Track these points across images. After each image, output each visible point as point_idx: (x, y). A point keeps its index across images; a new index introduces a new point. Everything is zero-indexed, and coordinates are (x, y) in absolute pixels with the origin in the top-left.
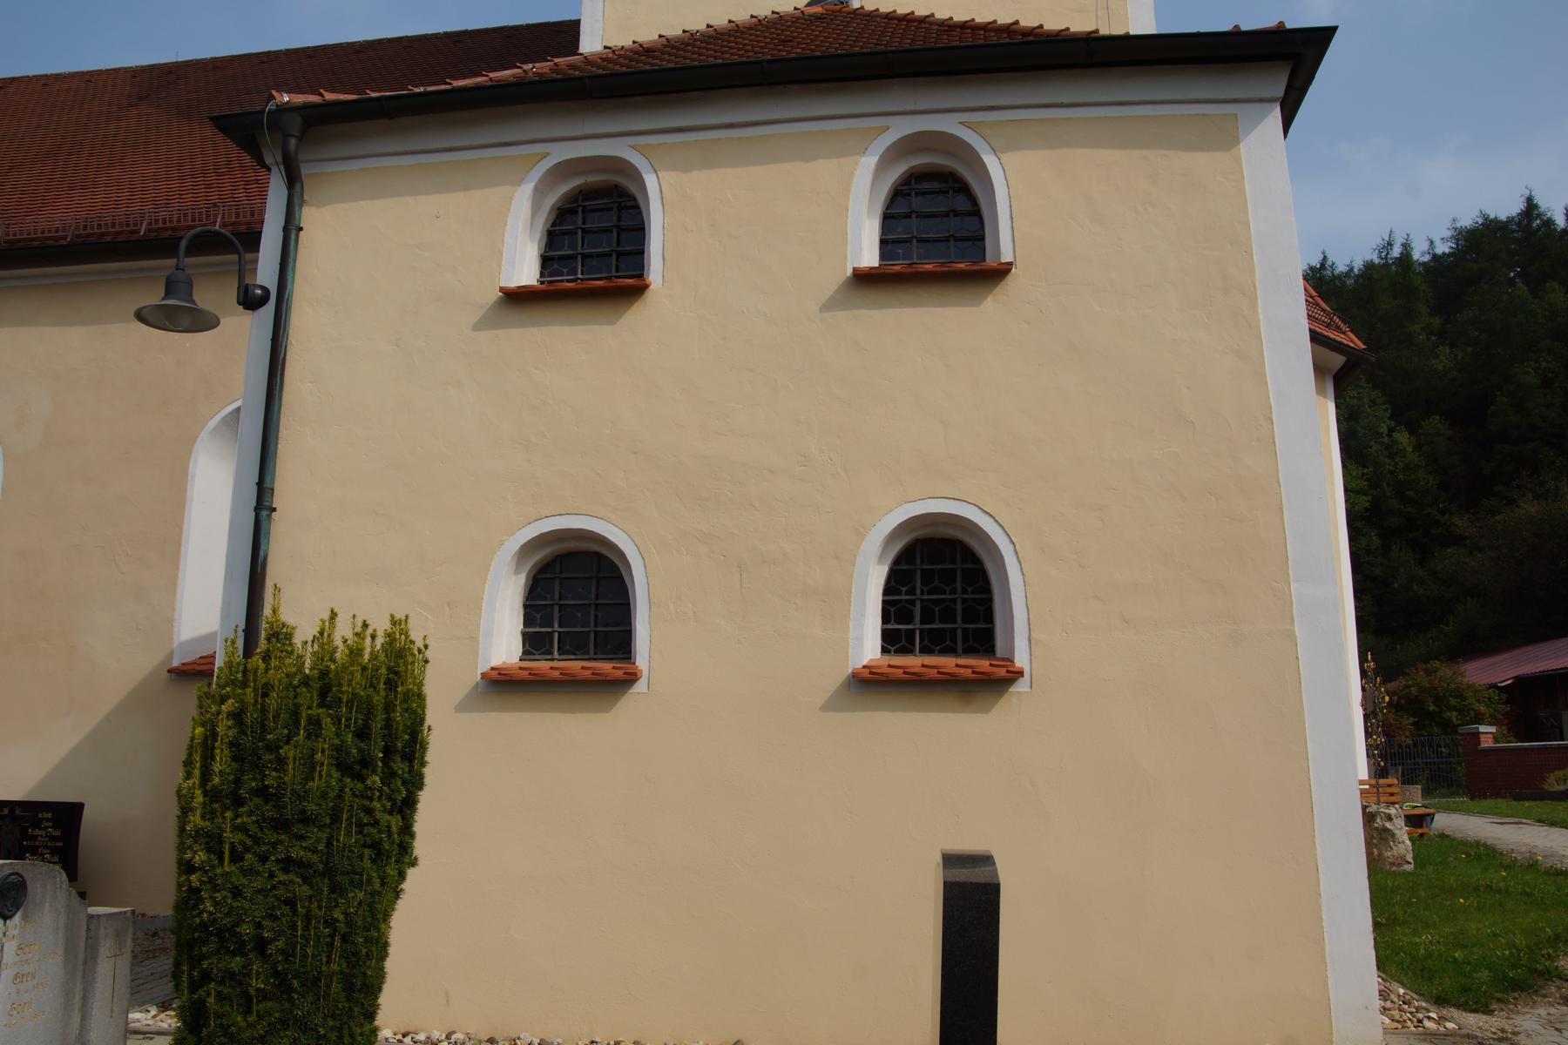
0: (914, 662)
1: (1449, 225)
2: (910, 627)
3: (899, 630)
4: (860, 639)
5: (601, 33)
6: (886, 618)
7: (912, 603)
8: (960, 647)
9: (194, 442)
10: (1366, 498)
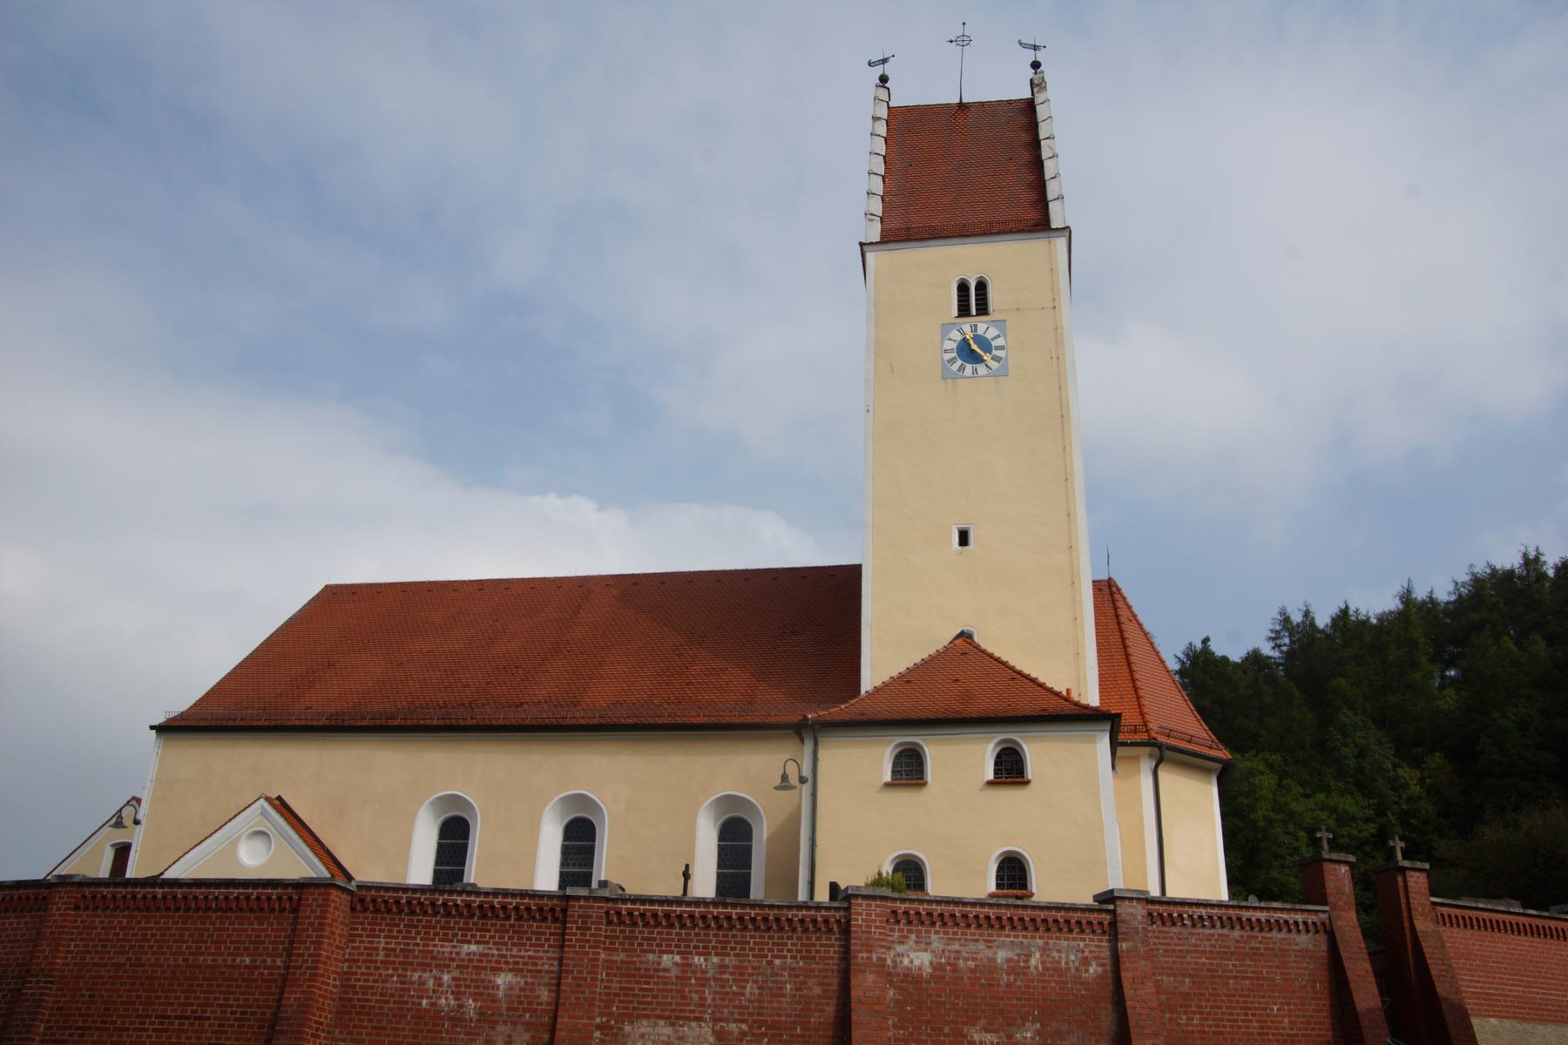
0: (1005, 891)
1: (1467, 571)
6: (997, 880)
10: (1372, 825)
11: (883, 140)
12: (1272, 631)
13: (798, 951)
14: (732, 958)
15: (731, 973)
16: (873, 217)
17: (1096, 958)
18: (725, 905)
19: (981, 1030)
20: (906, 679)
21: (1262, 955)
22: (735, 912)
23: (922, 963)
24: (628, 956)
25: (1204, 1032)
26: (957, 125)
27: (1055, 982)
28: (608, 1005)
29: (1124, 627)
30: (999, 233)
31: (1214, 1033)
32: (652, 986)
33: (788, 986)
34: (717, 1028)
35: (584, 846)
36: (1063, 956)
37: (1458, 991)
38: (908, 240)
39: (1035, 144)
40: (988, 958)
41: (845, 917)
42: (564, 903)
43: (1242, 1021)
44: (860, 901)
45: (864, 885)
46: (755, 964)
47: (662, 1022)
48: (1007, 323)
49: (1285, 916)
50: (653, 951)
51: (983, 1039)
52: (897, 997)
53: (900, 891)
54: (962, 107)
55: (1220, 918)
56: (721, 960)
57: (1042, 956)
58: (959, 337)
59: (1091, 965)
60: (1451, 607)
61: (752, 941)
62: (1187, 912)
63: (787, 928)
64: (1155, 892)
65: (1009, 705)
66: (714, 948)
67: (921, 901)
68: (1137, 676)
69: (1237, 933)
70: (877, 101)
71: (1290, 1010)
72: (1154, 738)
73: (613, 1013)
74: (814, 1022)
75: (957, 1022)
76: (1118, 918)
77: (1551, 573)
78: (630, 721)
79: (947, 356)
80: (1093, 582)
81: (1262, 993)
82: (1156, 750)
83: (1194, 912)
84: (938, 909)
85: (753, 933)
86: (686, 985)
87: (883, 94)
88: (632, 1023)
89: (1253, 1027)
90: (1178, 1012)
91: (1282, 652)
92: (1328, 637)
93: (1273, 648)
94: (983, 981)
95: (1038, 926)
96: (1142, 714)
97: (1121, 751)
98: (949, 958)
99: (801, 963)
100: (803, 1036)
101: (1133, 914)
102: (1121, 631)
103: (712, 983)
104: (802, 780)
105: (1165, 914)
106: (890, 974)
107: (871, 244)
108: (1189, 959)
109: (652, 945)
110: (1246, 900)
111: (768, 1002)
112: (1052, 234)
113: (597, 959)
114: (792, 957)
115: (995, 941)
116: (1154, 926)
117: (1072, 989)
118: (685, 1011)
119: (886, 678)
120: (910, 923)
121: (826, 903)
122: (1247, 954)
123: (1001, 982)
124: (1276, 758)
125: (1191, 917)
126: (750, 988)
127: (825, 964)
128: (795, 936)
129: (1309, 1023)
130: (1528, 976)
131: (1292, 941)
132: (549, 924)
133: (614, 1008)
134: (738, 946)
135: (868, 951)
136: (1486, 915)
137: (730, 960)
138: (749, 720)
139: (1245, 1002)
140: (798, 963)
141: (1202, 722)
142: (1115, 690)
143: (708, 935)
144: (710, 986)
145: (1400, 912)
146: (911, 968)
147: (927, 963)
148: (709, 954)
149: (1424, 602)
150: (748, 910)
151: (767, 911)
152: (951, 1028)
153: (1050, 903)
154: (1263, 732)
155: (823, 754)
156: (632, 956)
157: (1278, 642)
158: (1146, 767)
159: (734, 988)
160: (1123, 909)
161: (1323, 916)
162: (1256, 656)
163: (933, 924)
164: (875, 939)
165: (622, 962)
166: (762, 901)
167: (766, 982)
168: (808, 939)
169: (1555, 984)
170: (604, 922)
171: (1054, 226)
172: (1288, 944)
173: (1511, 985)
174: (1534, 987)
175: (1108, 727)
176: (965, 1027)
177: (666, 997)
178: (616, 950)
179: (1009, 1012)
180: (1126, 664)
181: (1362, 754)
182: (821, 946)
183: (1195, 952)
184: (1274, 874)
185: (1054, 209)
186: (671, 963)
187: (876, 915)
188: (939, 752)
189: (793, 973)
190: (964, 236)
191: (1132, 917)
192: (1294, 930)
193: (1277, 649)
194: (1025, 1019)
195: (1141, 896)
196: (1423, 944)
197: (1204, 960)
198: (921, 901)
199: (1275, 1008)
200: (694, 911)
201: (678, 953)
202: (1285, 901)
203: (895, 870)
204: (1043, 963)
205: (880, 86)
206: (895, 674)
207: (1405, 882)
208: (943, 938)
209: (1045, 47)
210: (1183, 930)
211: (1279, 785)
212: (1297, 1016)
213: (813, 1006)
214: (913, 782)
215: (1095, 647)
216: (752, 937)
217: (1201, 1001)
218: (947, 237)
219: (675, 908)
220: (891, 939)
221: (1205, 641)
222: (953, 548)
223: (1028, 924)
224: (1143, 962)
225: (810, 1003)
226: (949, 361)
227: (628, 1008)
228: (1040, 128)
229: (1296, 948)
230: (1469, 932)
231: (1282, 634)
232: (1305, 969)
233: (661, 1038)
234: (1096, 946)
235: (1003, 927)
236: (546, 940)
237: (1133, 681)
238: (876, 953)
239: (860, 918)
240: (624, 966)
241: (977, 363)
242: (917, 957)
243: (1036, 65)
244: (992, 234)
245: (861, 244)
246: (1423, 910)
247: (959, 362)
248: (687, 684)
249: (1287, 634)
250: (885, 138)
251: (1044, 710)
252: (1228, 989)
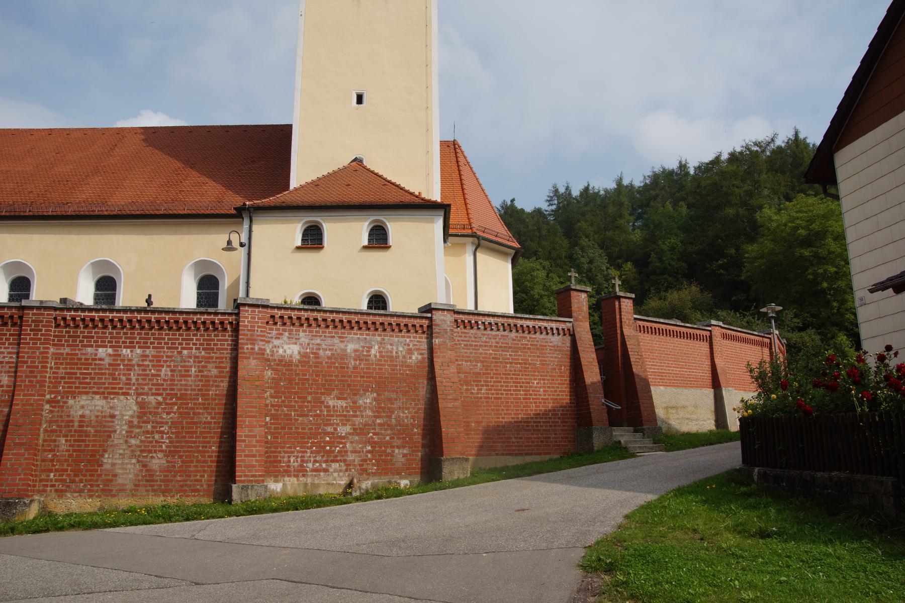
1: (650, 170)
13: (200, 344)
14: (151, 349)
15: (150, 361)
17: (417, 349)
19: (334, 398)
20: (315, 184)
21: (529, 349)
23: (293, 352)
24: (71, 350)
25: (488, 398)
27: (388, 365)
28: (56, 384)
29: (461, 168)
31: (495, 398)
32: (90, 371)
33: (193, 369)
34: (140, 400)
35: (109, 295)
36: (395, 348)
37: (645, 371)
40: (341, 349)
41: (236, 320)
42: (21, 312)
43: (514, 390)
44: (247, 308)
46: (169, 354)
47: (97, 397)
50: (92, 346)
51: (336, 404)
52: (273, 376)
55: (503, 324)
56: (143, 351)
57: (379, 348)
59: (414, 354)
60: (641, 189)
61: (166, 337)
63: (193, 328)
65: (380, 199)
66: (137, 343)
69: (513, 334)
71: (544, 383)
72: (475, 232)
73: (60, 391)
74: (212, 394)
75: (317, 393)
76: (433, 323)
77: (692, 172)
78: (138, 213)
81: (528, 373)
82: (476, 239)
85: (167, 332)
86: (116, 370)
88: (75, 398)
89: (521, 395)
90: (471, 385)
92: (578, 202)
93: (549, 206)
94: (337, 365)
98: (313, 349)
99: (203, 353)
100: (204, 404)
101: (443, 320)
102: (459, 171)
103: (136, 368)
104: (242, 245)
105: (466, 321)
106: (268, 360)
108: (481, 351)
109: (91, 341)
111: (178, 380)
113: (47, 353)
114: (196, 349)
115: (346, 337)
117: (400, 370)
118: (115, 388)
120: (284, 324)
122: (520, 348)
123: (350, 366)
124: (547, 263)
125: (483, 323)
126: (165, 372)
127: (221, 353)
128: (199, 333)
129: (555, 391)
130: (682, 362)
131: (549, 341)
132: (9, 327)
133: (61, 388)
134: (156, 341)
135: (251, 344)
136: (664, 327)
137: (150, 352)
139: (517, 379)
140: (201, 352)
143: (134, 334)
144: (135, 370)
145: (616, 323)
146: (285, 356)
147: (296, 352)
148: (134, 347)
149: (627, 186)
150: (163, 315)
151: (178, 316)
152: (313, 398)
154: (540, 250)
155: (255, 227)
156: (75, 350)
157: (551, 203)
158: (470, 249)
159: (153, 371)
160: (437, 317)
161: (569, 325)
163: (302, 325)
164: (258, 336)
165: (67, 354)
167: (177, 366)
168: (208, 335)
169: (696, 366)
170: (54, 325)
172: (547, 342)
173: (673, 367)
174: (685, 368)
175: (443, 213)
176: (323, 396)
177: (101, 379)
178: (63, 345)
179: (355, 385)
181: (591, 262)
182: (218, 340)
183: (485, 346)
186: (105, 354)
187: (259, 318)
188: (332, 228)
189: (197, 360)
192: (550, 334)
194: (366, 390)
196: (627, 343)
197: (491, 352)
199: (535, 382)
200: (123, 317)
201: (111, 347)
204: (379, 352)
206: (309, 180)
207: (620, 305)
208: (309, 335)
210: (478, 332)
211: (547, 276)
212: (549, 387)
213: (211, 383)
214: (315, 246)
215: (439, 152)
216: (166, 335)
217: (488, 378)
219: (108, 314)
220: (270, 336)
221: (513, 201)
224: (450, 352)
225: (208, 381)
227: (71, 387)
229: (551, 344)
230: (654, 336)
232: (555, 357)
233: (97, 408)
234: (418, 341)
235: (352, 328)
236: (7, 339)
238: (258, 345)
240: (69, 357)
242: (289, 348)
246: (629, 322)
252: (506, 370)
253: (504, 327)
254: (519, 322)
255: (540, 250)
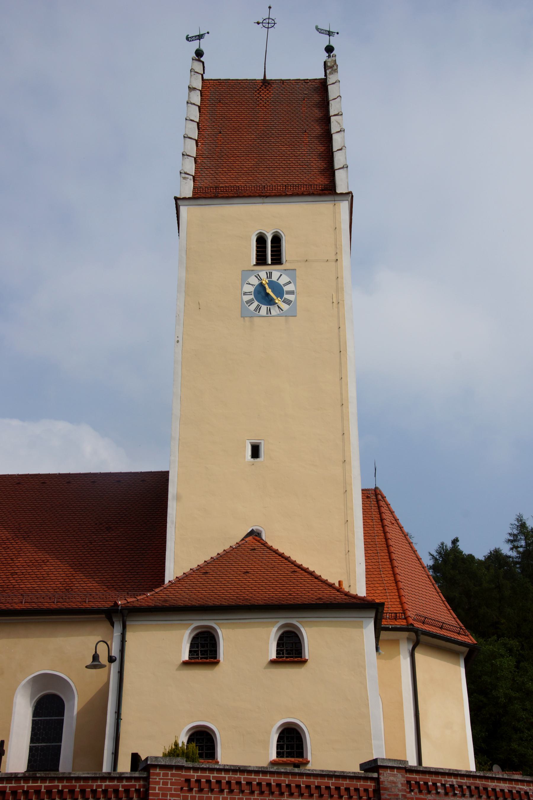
0: (285, 759)
2: (283, 751)
3: (281, 752)
4: (272, 753)
5: (174, 540)
6: (277, 748)
7: (284, 744)
8: (295, 757)
9: (16, 689)
11: (197, 108)
12: (510, 534)
16: (187, 176)
18: (35, 779)
22: (43, 786)
26: (261, 99)
29: (387, 529)
30: (292, 195)
38: (216, 197)
39: (326, 120)
41: (144, 786)
44: (158, 771)
45: (161, 755)
48: (298, 273)
49: (525, 788)
53: (193, 761)
54: (266, 82)
55: (469, 787)
58: (256, 282)
62: (440, 781)
64: (412, 762)
67: (212, 770)
68: (397, 571)
70: (193, 73)
72: (412, 625)
76: (381, 786)
79: (246, 298)
80: (362, 490)
82: (413, 635)
83: (445, 781)
84: (226, 776)
87: (198, 67)
91: (519, 552)
93: (512, 549)
95: (312, 792)
96: (402, 603)
97: (384, 635)
102: (385, 533)
104: (111, 660)
105: (422, 783)
107: (184, 199)
110: (491, 770)
112: (337, 198)
116: (413, 793)
119: (187, 570)
121: (127, 773)
124: (514, 643)
125: (443, 785)
138: (66, 606)
141: (451, 611)
142: (379, 582)
151: (74, 783)
153: (323, 771)
154: (503, 621)
157: (516, 544)
158: (405, 648)
160: (386, 777)
162: (497, 556)
166: (70, 773)
171: (339, 191)
175: (373, 615)
180: (388, 560)
184: (514, 746)
185: (340, 176)
190: (264, 196)
191: (393, 785)
193: (514, 549)
195: (401, 766)
198: (212, 770)
202: (525, 774)
203: (190, 740)
205: (196, 60)
206: (194, 566)
209: (338, 33)
211: (517, 667)
218: (249, 196)
221: (455, 541)
222: (246, 460)
223: (303, 790)
226: (247, 302)
228: (330, 105)
231: (519, 537)
237: (395, 574)
239: (157, 787)
241: (271, 305)
243: (329, 49)
244: (286, 195)
245: (176, 199)
247: (256, 303)
248: (12, 574)
249: (523, 537)
250: (199, 107)
251: (320, 599)
253: (470, 791)
254: (490, 784)
255: (503, 621)
